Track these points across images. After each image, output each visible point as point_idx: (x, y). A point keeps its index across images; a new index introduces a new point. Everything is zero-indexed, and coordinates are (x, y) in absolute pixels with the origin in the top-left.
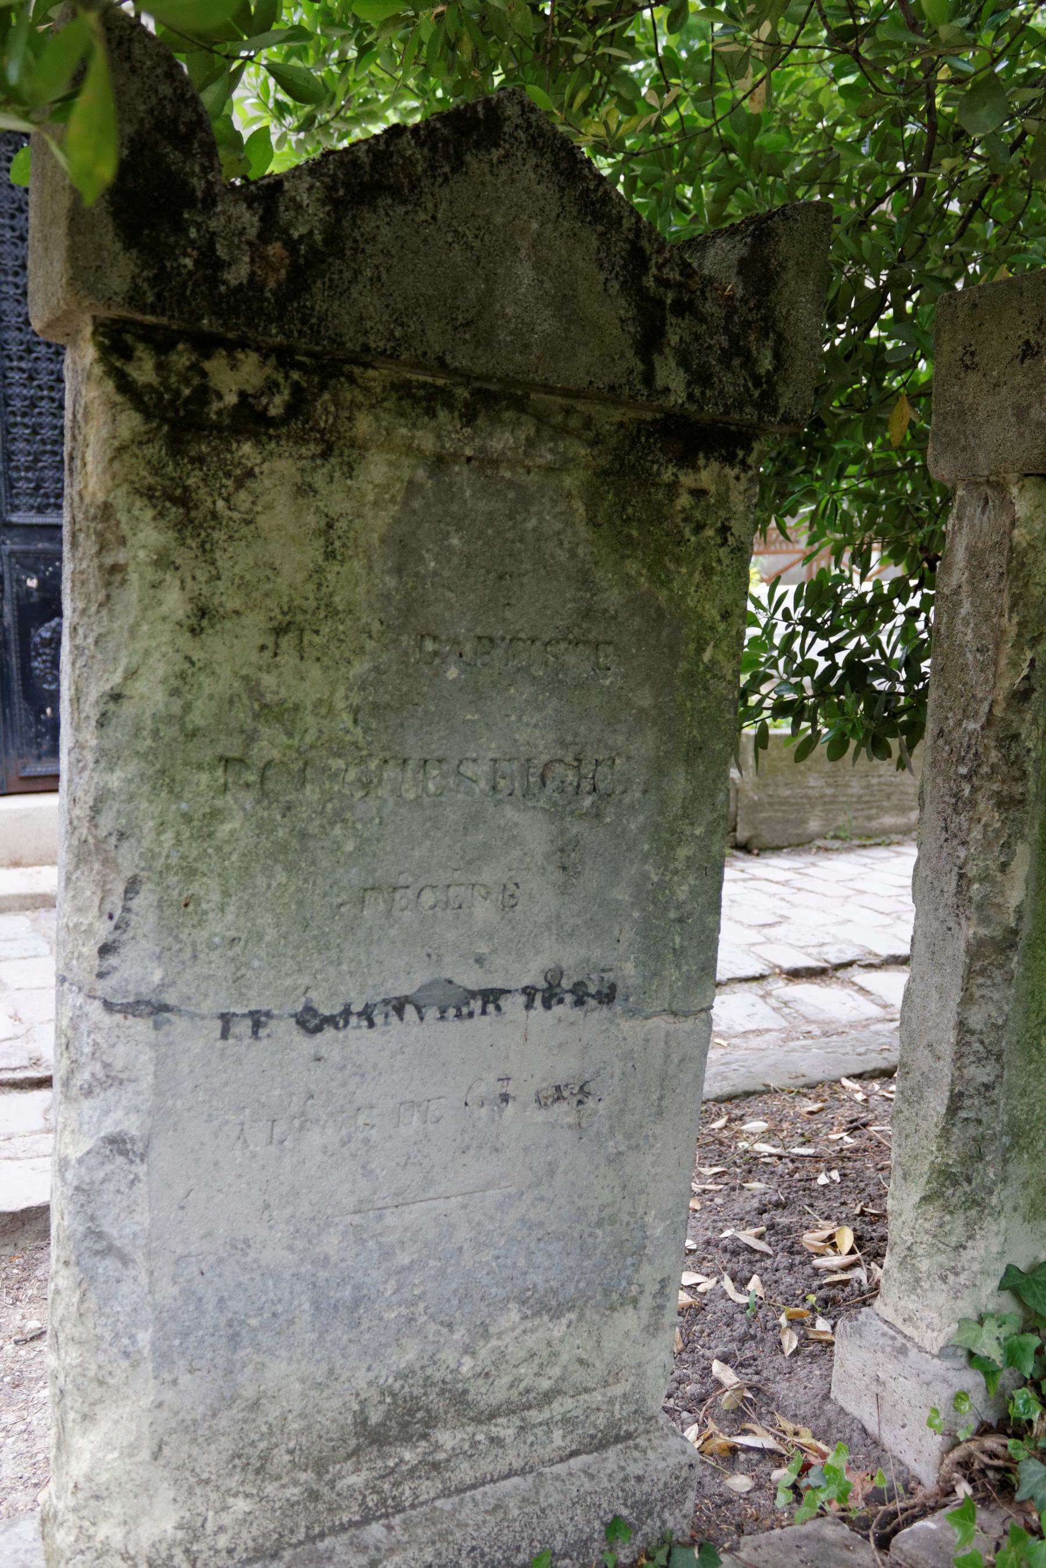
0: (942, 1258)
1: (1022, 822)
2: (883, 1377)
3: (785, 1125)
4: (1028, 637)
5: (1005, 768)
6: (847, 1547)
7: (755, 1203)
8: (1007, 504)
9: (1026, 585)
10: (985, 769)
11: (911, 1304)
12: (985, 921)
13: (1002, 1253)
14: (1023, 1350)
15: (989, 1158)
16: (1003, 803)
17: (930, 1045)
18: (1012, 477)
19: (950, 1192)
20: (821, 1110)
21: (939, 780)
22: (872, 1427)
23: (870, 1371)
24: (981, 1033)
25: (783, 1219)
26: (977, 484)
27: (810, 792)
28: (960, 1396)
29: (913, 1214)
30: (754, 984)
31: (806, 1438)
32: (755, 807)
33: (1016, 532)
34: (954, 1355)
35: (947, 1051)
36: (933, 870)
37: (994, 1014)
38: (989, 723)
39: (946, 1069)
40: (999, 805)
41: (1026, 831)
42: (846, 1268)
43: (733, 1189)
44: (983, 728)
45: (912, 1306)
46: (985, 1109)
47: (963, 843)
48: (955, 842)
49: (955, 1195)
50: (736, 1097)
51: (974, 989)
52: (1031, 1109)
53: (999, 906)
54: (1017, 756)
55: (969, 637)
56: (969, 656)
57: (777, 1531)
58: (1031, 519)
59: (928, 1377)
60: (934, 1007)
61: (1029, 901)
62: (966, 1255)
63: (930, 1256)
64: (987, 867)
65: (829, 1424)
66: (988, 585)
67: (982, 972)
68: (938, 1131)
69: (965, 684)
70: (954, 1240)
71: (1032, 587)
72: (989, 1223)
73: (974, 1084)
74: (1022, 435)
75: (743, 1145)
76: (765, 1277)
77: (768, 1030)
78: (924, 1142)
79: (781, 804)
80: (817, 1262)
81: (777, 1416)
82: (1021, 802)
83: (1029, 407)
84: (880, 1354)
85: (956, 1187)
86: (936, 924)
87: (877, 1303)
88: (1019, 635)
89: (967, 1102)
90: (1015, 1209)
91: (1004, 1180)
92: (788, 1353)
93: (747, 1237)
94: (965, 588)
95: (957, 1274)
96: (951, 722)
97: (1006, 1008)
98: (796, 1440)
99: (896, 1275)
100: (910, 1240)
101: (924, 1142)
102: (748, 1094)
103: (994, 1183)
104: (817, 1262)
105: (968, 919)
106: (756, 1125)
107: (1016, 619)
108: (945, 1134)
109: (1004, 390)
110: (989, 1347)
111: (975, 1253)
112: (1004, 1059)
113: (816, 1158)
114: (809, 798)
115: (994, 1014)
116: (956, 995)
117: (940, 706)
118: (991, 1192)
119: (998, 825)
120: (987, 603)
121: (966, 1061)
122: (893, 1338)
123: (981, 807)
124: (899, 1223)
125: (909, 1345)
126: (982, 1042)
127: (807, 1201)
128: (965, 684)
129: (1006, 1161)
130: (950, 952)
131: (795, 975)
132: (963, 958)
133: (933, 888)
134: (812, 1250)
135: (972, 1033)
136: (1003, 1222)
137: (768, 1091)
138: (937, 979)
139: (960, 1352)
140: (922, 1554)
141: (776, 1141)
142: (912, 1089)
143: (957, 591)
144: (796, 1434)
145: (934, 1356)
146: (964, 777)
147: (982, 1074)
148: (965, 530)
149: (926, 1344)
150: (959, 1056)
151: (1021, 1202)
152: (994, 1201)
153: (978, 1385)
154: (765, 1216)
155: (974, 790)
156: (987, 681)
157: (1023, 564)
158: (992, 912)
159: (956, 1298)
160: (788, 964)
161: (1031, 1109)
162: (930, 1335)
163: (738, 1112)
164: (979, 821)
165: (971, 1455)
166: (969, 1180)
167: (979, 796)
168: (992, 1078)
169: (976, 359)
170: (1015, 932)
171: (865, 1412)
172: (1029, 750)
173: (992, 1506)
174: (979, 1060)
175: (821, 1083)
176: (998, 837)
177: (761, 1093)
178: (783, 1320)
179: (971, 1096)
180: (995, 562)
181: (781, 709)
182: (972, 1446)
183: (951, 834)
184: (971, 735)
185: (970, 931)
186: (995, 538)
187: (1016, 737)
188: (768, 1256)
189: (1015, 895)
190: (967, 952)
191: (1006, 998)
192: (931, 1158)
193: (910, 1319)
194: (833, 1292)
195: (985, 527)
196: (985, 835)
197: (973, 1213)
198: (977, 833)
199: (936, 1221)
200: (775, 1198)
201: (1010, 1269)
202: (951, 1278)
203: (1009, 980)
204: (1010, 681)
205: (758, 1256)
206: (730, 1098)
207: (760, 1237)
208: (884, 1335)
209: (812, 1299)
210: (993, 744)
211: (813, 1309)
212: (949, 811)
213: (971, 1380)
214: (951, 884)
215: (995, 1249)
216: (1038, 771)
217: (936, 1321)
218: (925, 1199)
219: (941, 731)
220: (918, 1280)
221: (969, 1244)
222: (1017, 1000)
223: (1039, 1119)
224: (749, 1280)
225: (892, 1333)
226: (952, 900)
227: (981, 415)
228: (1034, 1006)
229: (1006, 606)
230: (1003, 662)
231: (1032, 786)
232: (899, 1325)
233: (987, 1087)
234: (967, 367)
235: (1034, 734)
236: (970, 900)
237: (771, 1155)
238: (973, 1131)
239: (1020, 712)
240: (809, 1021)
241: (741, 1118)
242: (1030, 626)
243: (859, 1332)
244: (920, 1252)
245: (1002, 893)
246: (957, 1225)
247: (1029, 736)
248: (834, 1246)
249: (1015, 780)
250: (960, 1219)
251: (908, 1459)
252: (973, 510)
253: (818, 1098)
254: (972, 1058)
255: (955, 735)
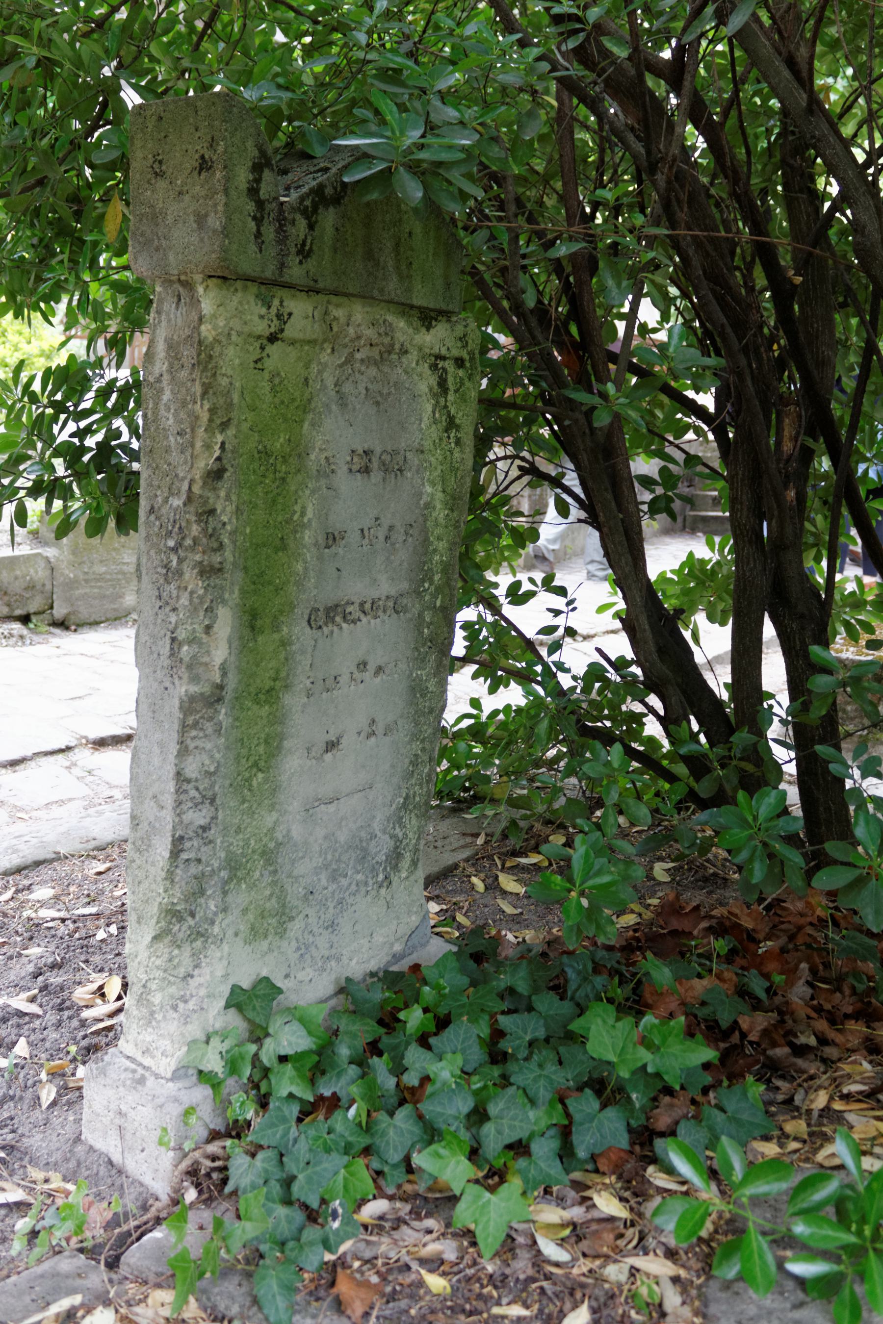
0: (172, 990)
1: (222, 588)
2: (124, 1108)
3: (72, 889)
4: (218, 422)
5: (204, 540)
6: (79, 1275)
7: (31, 968)
8: (195, 302)
9: (214, 375)
10: (188, 542)
11: (148, 1036)
12: (195, 679)
13: (226, 976)
14: (243, 1058)
15: (209, 892)
16: (207, 571)
17: (155, 797)
18: (198, 277)
19: (177, 928)
20: (109, 869)
21: (152, 552)
22: (116, 1158)
23: (113, 1106)
24: (197, 780)
25: (55, 979)
26: (171, 282)
27: (125, 568)
28: (189, 1112)
29: (146, 954)
30: (60, 756)
31: (56, 1183)
32: (71, 585)
33: (203, 328)
34: (186, 1075)
35: (168, 800)
36: (152, 636)
37: (207, 762)
38: (189, 500)
39: (168, 816)
40: (201, 573)
41: (227, 596)
42: (111, 1015)
43: (11, 958)
44: (185, 504)
45: (149, 1038)
46: (203, 849)
47: (174, 610)
48: (168, 609)
49: (181, 930)
50: (25, 868)
51: (189, 741)
52: (247, 842)
53: (206, 664)
54: (214, 529)
55: (171, 422)
56: (172, 439)
57: (14, 1278)
58: (214, 316)
59: (159, 1101)
60: (156, 761)
61: (233, 658)
62: (193, 983)
63: (161, 989)
64: (194, 630)
65: (79, 1164)
66: (183, 374)
67: (195, 725)
68: (163, 874)
69: (169, 464)
70: (182, 971)
71: (219, 378)
72: (214, 953)
73: (193, 828)
74: (202, 240)
75: (27, 913)
76: (32, 1038)
77: (70, 800)
78: (154, 886)
79: (98, 580)
80: (86, 1014)
81: (29, 1168)
82: (220, 570)
83: (206, 215)
84: (121, 1089)
85: (183, 923)
86: (155, 685)
87: (121, 1043)
88: (211, 420)
89: (188, 845)
90: (236, 935)
91: (225, 910)
92: (45, 1105)
93: (20, 1002)
94: (166, 377)
95: (186, 1002)
96: (160, 499)
97: (217, 756)
98: (46, 1186)
99: (135, 1012)
100: (144, 977)
101: (154, 886)
102: (38, 864)
103: (216, 914)
104: (86, 1014)
105: (180, 678)
106: (43, 893)
107: (207, 406)
108: (170, 876)
109: (187, 198)
110: (214, 1064)
111: (201, 980)
112: (218, 801)
113: (97, 916)
114: (124, 574)
115: (207, 762)
116: (174, 748)
117: (150, 485)
118: (213, 923)
119: (201, 592)
120: (184, 390)
121: (184, 807)
122: (134, 1071)
123: (187, 576)
124: (135, 964)
125: (147, 1074)
126: (197, 789)
127: (83, 958)
128: (169, 464)
129: (225, 893)
130: (167, 710)
131: (101, 743)
132: (178, 714)
133: (152, 653)
134: (82, 1003)
135: (188, 781)
136: (226, 948)
137: (59, 858)
138: (158, 736)
139: (191, 1072)
140: (147, 1263)
141: (61, 906)
142: (142, 839)
143: (159, 380)
144: (46, 1181)
145: (168, 1080)
146: (172, 549)
147: (198, 817)
148: (164, 324)
149: (161, 1071)
150: (179, 803)
151: (242, 927)
152: (216, 930)
153: (205, 1098)
154: (40, 978)
155: (181, 561)
156: (186, 463)
157: (211, 357)
158: (201, 670)
159: (186, 1023)
160: (96, 733)
161: (247, 842)
162: (165, 1061)
163: (26, 882)
164: (186, 588)
165: (196, 1163)
166: (193, 915)
167: (185, 566)
168: (208, 820)
169: (164, 168)
170: (221, 687)
171: (108, 1144)
172: (224, 524)
173: (214, 1204)
174: (196, 805)
175: (112, 844)
176: (202, 603)
177: (51, 861)
178: (43, 1076)
179: (190, 839)
180: (188, 353)
181: (35, 491)
182: (197, 1154)
183: (164, 603)
184: (176, 510)
185: (182, 688)
186: (187, 332)
187: (212, 512)
188: (38, 1016)
189: (220, 653)
190: (181, 708)
191: (216, 746)
192: (159, 900)
193: (148, 1050)
194: (95, 1040)
195: (179, 321)
196: (191, 601)
197: (198, 944)
198: (184, 600)
199: (166, 956)
200: (51, 960)
201: (236, 989)
202: (181, 1006)
203: (218, 731)
204: (205, 462)
205: (27, 1019)
206: (19, 870)
207: (32, 1000)
208: (126, 1070)
209: (73, 1049)
210: (194, 518)
211: (74, 1060)
212: (162, 581)
213: (201, 1094)
214: (165, 647)
215: (219, 973)
216: (234, 542)
217: (169, 1048)
218: (156, 938)
219: (152, 508)
220: (152, 1013)
221: (196, 972)
222: (227, 748)
223: (254, 852)
224: (14, 1044)
225: (133, 1066)
226: (167, 662)
227: (170, 220)
228: (244, 752)
229: (198, 394)
230: (199, 444)
231: (228, 554)
232: (139, 1058)
233: (204, 828)
234: (156, 174)
235: (228, 509)
236: (181, 660)
237: (53, 920)
238: (194, 870)
239: (215, 489)
240: (111, 787)
241: (29, 888)
242: (220, 413)
243: (103, 1072)
244: (154, 987)
245: (208, 652)
246: (185, 957)
247: (223, 511)
248: (103, 995)
249: (215, 550)
250: (187, 950)
251: (147, 1180)
252: (169, 306)
253: (107, 858)
254: (190, 804)
255: (164, 511)
